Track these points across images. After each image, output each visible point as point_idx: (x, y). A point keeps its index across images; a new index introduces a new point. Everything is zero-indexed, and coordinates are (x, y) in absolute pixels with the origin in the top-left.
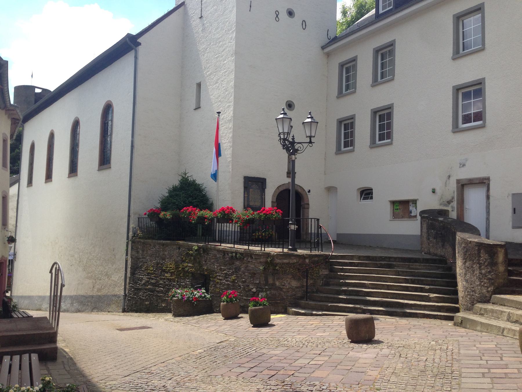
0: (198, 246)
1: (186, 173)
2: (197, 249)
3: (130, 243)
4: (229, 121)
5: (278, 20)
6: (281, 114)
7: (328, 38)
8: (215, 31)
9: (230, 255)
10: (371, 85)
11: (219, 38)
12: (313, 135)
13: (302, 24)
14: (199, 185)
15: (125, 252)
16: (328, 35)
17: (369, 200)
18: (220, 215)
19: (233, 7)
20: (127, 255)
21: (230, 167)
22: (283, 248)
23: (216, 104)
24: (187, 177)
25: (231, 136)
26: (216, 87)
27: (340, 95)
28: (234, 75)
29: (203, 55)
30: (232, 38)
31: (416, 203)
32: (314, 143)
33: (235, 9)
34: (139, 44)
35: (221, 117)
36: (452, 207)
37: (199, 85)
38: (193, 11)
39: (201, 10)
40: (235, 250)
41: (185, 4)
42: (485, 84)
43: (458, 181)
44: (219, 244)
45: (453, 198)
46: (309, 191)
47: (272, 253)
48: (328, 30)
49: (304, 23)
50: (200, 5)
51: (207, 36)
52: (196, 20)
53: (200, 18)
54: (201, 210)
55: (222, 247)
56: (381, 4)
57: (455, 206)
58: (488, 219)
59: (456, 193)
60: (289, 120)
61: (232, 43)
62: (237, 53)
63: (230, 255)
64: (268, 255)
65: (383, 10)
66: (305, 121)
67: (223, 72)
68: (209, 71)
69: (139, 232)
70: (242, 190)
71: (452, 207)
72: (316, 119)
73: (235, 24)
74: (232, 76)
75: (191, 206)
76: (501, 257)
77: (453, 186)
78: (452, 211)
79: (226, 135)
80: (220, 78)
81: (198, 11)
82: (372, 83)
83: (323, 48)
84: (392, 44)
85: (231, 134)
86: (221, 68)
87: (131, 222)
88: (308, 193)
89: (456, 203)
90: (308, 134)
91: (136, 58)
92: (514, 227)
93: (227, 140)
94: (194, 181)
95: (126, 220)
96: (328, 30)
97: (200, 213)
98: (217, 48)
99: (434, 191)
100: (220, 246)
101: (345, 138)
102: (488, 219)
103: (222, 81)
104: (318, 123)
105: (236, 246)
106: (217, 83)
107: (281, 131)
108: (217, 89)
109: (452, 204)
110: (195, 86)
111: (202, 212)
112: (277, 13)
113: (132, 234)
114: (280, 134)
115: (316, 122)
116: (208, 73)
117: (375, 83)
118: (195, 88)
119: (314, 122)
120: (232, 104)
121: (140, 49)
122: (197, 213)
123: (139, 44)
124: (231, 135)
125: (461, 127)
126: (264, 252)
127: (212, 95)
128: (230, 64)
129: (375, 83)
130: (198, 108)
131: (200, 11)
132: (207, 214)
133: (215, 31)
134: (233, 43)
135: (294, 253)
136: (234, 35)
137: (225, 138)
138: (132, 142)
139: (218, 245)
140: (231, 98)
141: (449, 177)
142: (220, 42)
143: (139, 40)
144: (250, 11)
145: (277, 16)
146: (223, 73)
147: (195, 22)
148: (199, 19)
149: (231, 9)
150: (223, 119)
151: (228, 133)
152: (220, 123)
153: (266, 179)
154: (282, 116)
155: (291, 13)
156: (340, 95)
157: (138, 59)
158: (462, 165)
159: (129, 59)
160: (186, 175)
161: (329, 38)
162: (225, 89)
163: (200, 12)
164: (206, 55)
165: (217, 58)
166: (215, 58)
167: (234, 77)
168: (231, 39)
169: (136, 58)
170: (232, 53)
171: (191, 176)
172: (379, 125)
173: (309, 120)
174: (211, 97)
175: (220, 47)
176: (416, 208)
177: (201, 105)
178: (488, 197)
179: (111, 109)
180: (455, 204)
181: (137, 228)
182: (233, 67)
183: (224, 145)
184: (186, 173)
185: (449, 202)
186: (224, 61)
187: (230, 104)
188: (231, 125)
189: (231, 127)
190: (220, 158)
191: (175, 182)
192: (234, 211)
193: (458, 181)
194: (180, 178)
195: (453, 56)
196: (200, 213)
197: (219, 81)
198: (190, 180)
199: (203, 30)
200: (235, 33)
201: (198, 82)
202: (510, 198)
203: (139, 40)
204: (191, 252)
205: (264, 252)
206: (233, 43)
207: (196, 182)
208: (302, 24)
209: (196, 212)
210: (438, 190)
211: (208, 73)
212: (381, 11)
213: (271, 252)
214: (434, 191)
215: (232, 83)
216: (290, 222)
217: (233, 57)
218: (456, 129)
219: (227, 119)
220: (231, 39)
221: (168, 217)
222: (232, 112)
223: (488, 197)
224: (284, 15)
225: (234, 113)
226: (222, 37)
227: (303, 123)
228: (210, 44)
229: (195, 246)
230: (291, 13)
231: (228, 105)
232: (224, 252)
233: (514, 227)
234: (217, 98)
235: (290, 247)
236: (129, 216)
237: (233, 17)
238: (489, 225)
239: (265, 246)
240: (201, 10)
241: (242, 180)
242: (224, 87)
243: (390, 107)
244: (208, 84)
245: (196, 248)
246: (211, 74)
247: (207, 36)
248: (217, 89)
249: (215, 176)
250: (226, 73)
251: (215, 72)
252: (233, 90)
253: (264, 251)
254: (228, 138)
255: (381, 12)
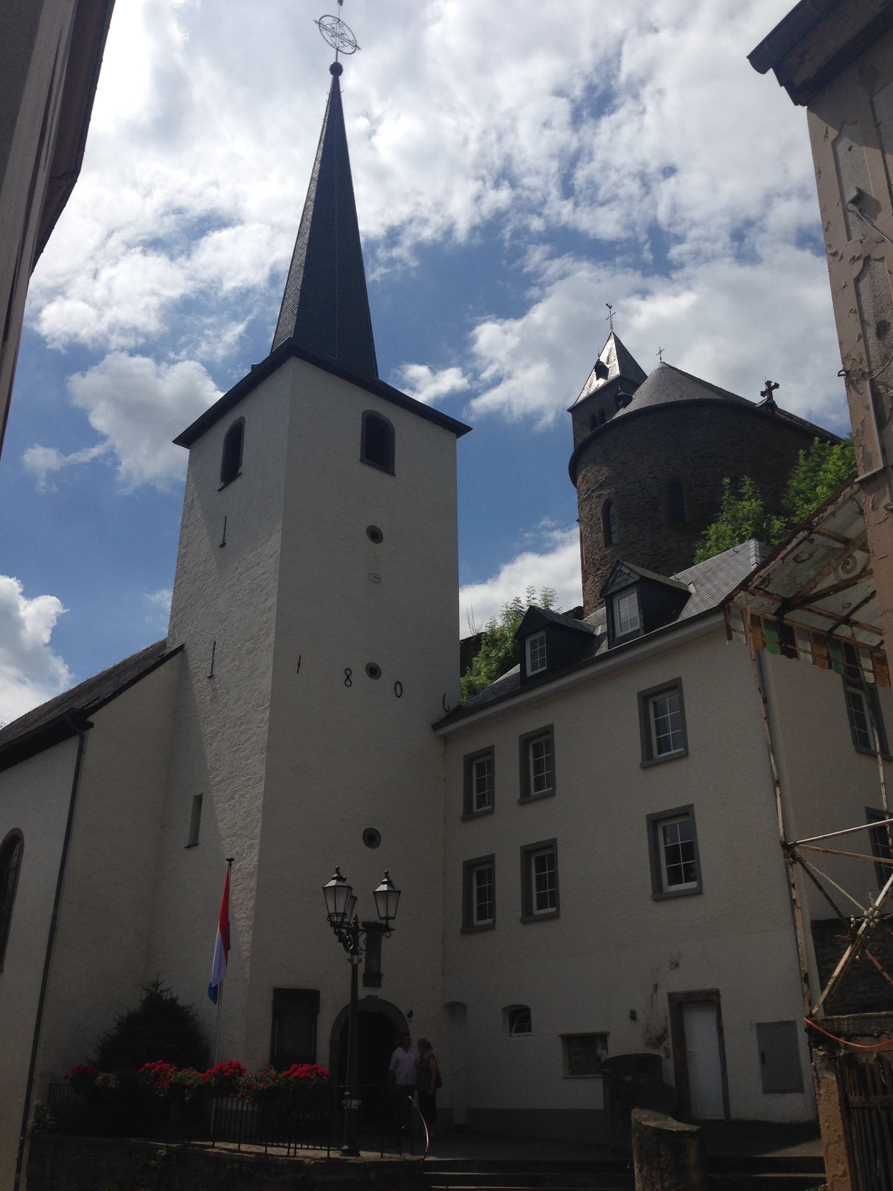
0: (168, 1149)
1: (159, 983)
2: (165, 1156)
3: (28, 1143)
4: (250, 875)
5: (348, 684)
6: (333, 879)
7: (444, 709)
8: (234, 704)
9: (229, 1167)
10: (518, 800)
11: (240, 718)
12: (391, 914)
13: (395, 688)
14: (183, 1008)
15: (15, 1166)
16: (444, 703)
17: (525, 1034)
18: (214, 1079)
19: (268, 667)
20: (18, 1171)
21: (247, 970)
22: (329, 1150)
23: (228, 840)
24: (158, 991)
25: (251, 905)
26: (231, 807)
27: (468, 815)
28: (263, 786)
29: (211, 745)
30: (263, 719)
31: (606, 1042)
32: (394, 930)
33: (271, 669)
34: (91, 725)
35: (236, 866)
36: (667, 1050)
37: (199, 800)
38: (197, 663)
39: (213, 663)
40: (239, 1156)
41: (185, 649)
42: (693, 815)
43: (672, 997)
44: (210, 1143)
45: (666, 1030)
46: (410, 1015)
47: (307, 1161)
48: (445, 695)
49: (398, 686)
50: (212, 654)
51: (220, 711)
52: (202, 681)
53: (210, 677)
54: (179, 1070)
55: (215, 1150)
56: (530, 660)
57: (671, 1047)
58: (724, 1074)
59: (669, 1021)
60: (347, 889)
61: (262, 729)
62: (270, 748)
63: (229, 1167)
64: (298, 1165)
65: (532, 671)
66: (376, 890)
67: (243, 779)
68: (219, 776)
69: (48, 1117)
70: (269, 1020)
71: (667, 1050)
72: (398, 886)
73: (270, 697)
74: (260, 789)
75: (160, 1061)
76: (693, 1157)
77: (663, 1006)
78: (667, 1057)
79: (242, 903)
80: (238, 790)
81: (207, 665)
82: (521, 797)
83: (436, 727)
84: (548, 731)
85: (253, 902)
86: (240, 772)
87: (34, 1095)
88: (407, 1018)
89: (670, 1039)
90: (383, 914)
91: (81, 751)
92: (767, 1091)
93: (244, 913)
94: (173, 1000)
95: (23, 1090)
96: (445, 695)
97: (175, 1075)
98: (236, 734)
99: (633, 1016)
100: (213, 1147)
101: (479, 900)
102: (724, 1074)
103: (242, 796)
104: (399, 892)
105: (244, 1147)
106: (232, 798)
107: (332, 910)
108: (231, 810)
109: (665, 1043)
110: (191, 801)
111: (180, 1073)
112: (348, 673)
113: (34, 1123)
114: (330, 915)
115: (396, 891)
116: (216, 779)
117: (526, 797)
118: (191, 805)
119: (393, 893)
120: (257, 841)
121: (92, 736)
122: (171, 1077)
123: (91, 725)
124: (251, 904)
125: (666, 891)
126: (295, 1159)
127: (221, 821)
128: (258, 766)
129: (526, 797)
130: (193, 844)
131: (210, 664)
132: (191, 1076)
133: (234, 704)
134: (264, 729)
135: (349, 1160)
136: (267, 715)
137: (241, 909)
138: (55, 918)
139: (209, 1147)
140: (255, 831)
141: (656, 987)
142: (242, 724)
143: (91, 719)
144: (298, 672)
145: (348, 677)
146: (244, 781)
147: (200, 683)
148: (206, 680)
149: (263, 670)
150: (239, 870)
151: (246, 899)
152: (233, 878)
153: (521, 847)
154: (333, 883)
155: (373, 671)
156: (468, 815)
157: (84, 753)
158: (673, 966)
159: (67, 751)
160: (157, 988)
161: (447, 709)
162: (246, 812)
163: (211, 668)
164: (215, 744)
165: (234, 752)
166: (232, 751)
167: (263, 790)
168: (261, 722)
169: (81, 751)
170: (261, 747)
171: (167, 990)
172: (537, 876)
173: (384, 888)
174: (220, 825)
175: (242, 733)
176: (607, 1052)
177: (200, 840)
178: (720, 1030)
179: (18, 846)
180: (669, 1043)
181: (45, 1107)
182: (262, 772)
183: (241, 923)
184: (159, 983)
185: (660, 1039)
186: (246, 760)
187: (253, 841)
188: (253, 883)
189: (253, 888)
190: (229, 952)
191: (134, 1001)
192: (241, 1071)
193: (672, 997)
194: (145, 995)
195: (642, 762)
196: (175, 1075)
197: (237, 796)
198: (164, 998)
199: (214, 699)
200: (268, 712)
201: (197, 793)
202: (754, 1031)
203: (91, 719)
204: (153, 1162)
205: (295, 1159)
206: (264, 729)
207: (178, 1003)
208: (395, 688)
209: (169, 1074)
210: (640, 1015)
211: (216, 779)
212: (529, 673)
213: (303, 1160)
214: (633, 1016)
215: (260, 802)
216: (347, 1093)
217: (263, 754)
218: (659, 895)
219: (247, 870)
220: (261, 722)
221: (113, 1084)
222: (256, 858)
223: (720, 1030)
224: (360, 676)
225: (260, 861)
226: (245, 715)
227: (375, 893)
228: (224, 725)
229: (162, 1149)
230: (373, 671)
231: (249, 842)
232: (219, 1160)
233: (767, 1091)
234: (230, 828)
235: (346, 1147)
236: (31, 1081)
237: (266, 683)
238: (727, 1086)
239: (289, 1145)
240: (213, 663)
241: (269, 997)
242: (244, 807)
243: (551, 845)
244: (215, 799)
245: (163, 1152)
246: (223, 780)
247: (220, 711)
248: (231, 810)
249: (214, 993)
250: (250, 782)
251: (229, 778)
252: (259, 815)
253: (295, 1156)
254: (247, 909)
255: (530, 675)
